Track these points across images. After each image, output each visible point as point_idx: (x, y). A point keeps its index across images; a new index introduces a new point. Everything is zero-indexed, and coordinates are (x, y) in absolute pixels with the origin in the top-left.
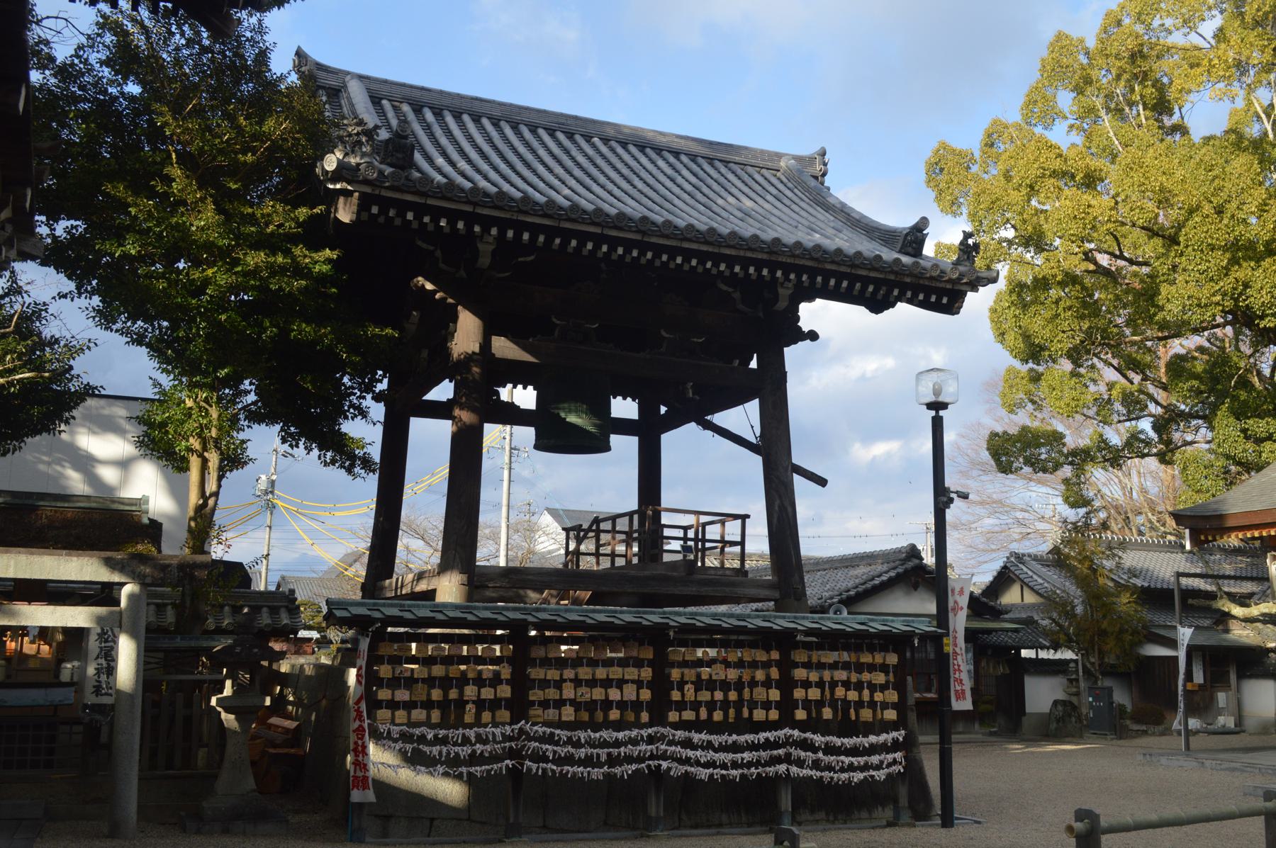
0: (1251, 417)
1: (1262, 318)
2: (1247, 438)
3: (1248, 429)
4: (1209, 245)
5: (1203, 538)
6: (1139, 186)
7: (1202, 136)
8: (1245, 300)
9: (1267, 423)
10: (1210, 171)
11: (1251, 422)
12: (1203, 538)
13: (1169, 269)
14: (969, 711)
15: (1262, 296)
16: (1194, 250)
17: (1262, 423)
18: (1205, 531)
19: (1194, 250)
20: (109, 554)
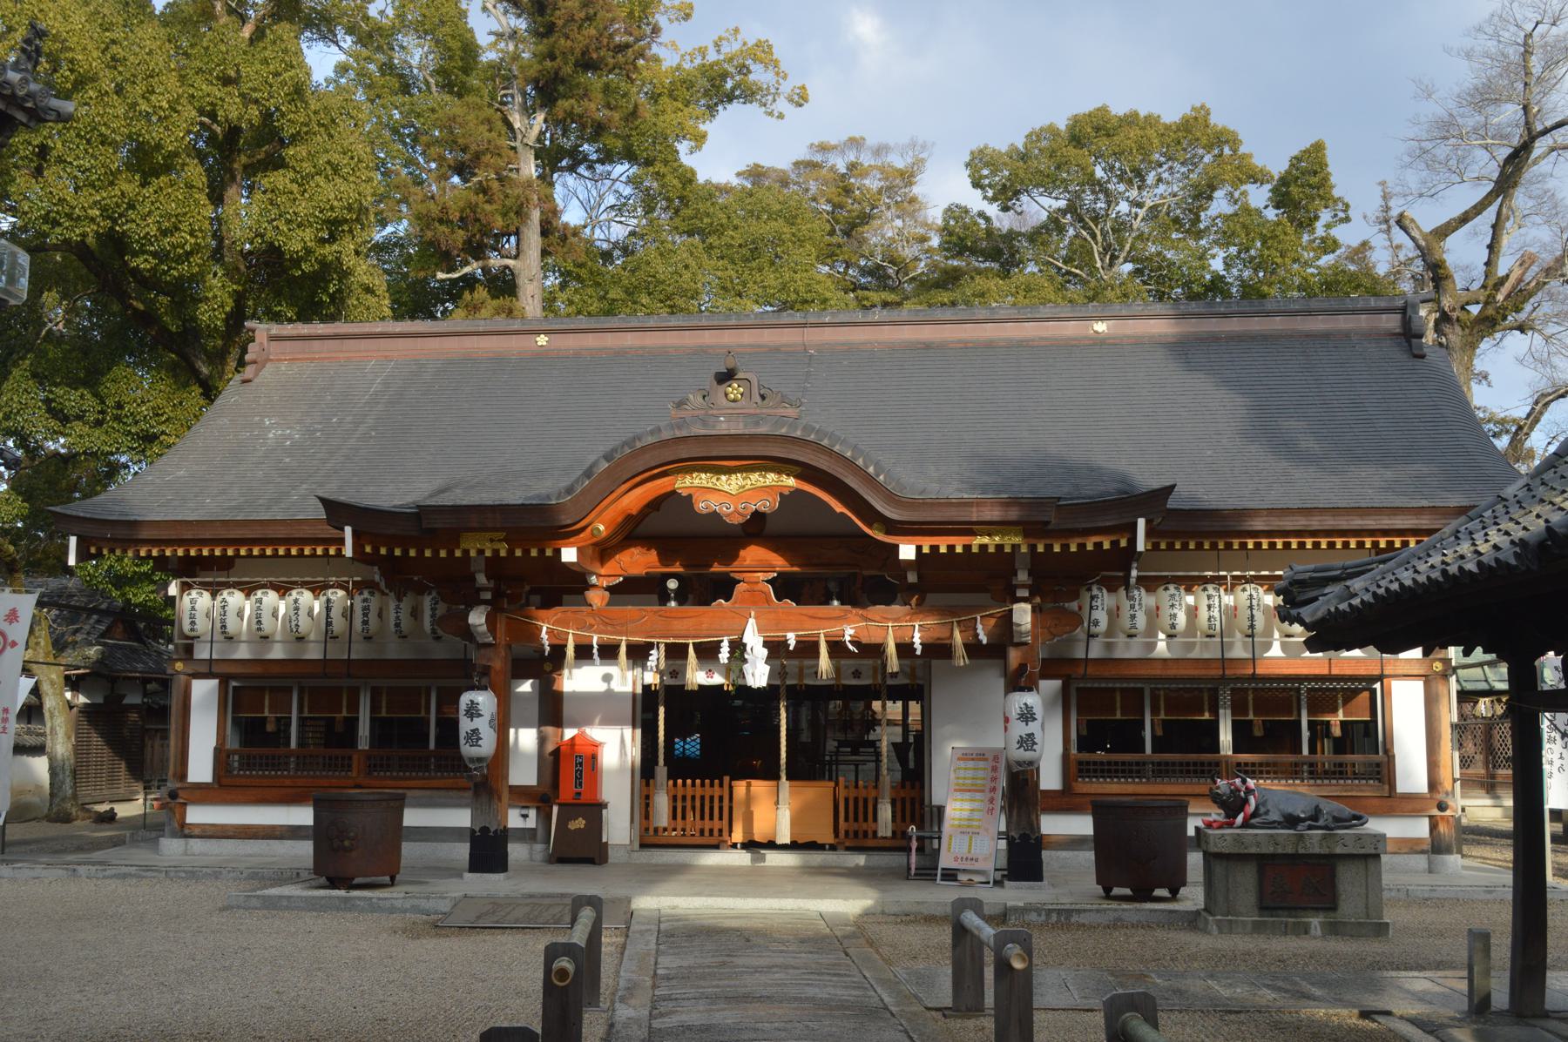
0: (60, 384)
1: (135, 254)
2: (50, 410)
3: (53, 400)
4: (101, 135)
5: (93, 550)
6: (41, 11)
7: (1523, 336)
8: (123, 224)
9: (82, 396)
10: (107, 30)
11: (59, 391)
12: (93, 550)
13: (33, 153)
14: (938, 658)
15: (148, 225)
16: (78, 135)
17: (75, 395)
18: (100, 541)
19: (78, 135)
20: (185, 579)
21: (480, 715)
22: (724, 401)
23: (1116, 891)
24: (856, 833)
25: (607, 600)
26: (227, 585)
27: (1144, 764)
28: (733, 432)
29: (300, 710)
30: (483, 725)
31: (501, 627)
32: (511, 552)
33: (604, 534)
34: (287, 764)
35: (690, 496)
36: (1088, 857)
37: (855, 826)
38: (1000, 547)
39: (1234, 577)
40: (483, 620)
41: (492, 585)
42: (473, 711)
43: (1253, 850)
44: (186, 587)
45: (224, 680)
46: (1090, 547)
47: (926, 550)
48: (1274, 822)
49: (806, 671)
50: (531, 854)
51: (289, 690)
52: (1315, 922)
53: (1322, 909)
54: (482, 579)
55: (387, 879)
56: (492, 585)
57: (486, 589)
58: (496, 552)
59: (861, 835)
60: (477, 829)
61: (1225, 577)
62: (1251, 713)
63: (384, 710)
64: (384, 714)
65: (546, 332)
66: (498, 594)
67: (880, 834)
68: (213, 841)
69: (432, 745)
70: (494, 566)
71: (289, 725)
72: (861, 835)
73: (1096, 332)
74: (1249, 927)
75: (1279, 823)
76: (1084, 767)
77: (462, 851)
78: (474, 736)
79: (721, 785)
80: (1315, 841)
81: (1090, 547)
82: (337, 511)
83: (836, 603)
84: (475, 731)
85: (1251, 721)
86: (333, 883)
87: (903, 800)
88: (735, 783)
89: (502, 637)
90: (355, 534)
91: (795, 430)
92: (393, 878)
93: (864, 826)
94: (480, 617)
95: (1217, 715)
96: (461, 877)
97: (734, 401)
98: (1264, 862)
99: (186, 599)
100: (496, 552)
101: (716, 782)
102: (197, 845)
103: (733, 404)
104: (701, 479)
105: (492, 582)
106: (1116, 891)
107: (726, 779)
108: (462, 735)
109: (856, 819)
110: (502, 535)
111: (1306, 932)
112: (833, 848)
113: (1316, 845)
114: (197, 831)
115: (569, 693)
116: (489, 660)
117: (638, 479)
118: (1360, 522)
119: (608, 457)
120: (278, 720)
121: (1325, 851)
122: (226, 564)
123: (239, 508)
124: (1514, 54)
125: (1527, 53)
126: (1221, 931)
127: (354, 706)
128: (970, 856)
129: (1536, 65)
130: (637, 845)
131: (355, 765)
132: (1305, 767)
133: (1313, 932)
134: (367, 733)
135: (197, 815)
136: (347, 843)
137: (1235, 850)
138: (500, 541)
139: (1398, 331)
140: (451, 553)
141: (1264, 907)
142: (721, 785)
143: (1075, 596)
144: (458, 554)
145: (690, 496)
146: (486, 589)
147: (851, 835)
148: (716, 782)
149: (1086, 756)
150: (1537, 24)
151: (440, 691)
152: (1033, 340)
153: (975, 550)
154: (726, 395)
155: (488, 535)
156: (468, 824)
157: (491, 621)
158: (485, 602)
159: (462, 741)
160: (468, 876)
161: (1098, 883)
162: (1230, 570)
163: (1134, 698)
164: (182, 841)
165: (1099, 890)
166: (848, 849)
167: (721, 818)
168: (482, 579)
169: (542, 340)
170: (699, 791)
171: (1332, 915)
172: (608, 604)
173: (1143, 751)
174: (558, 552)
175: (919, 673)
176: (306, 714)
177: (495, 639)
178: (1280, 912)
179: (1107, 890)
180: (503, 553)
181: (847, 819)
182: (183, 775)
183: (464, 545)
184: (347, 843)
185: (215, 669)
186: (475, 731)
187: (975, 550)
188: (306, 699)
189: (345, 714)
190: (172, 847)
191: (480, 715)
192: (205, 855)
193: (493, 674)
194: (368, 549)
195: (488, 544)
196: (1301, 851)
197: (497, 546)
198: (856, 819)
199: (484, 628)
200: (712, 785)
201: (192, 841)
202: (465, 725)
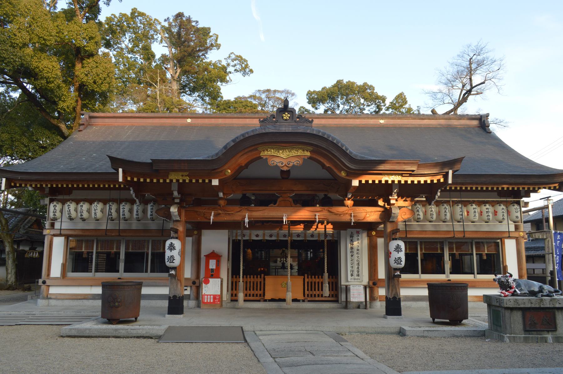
12: (13, 184)
21: (175, 249)
22: (282, 120)
23: (436, 320)
24: (311, 295)
25: (226, 203)
26: (68, 200)
28: (287, 131)
29: (97, 249)
30: (175, 253)
31: (183, 214)
32: (191, 181)
33: (230, 174)
35: (266, 159)
36: (426, 305)
37: (311, 293)
38: (387, 181)
39: (453, 201)
40: (176, 210)
41: (180, 196)
42: (172, 247)
43: (522, 306)
44: (51, 201)
45: (67, 237)
47: (363, 182)
48: (525, 293)
49: (293, 235)
51: (93, 241)
52: (549, 336)
53: (551, 331)
54: (176, 194)
55: (134, 319)
56: (180, 197)
57: (177, 198)
58: (184, 181)
59: (313, 296)
60: (172, 296)
62: (455, 250)
63: (130, 249)
65: (190, 118)
66: (182, 200)
67: (324, 296)
70: (181, 186)
71: (92, 256)
72: (313, 296)
73: (381, 123)
74: (522, 339)
75: (527, 294)
77: (165, 304)
78: (172, 258)
79: (261, 277)
80: (548, 302)
82: (116, 162)
83: (318, 206)
84: (172, 257)
85: (455, 253)
86: (111, 321)
87: (332, 283)
88: (266, 277)
89: (183, 218)
90: (123, 171)
91: (129, 250)
92: (136, 319)
93: (314, 293)
94: (175, 209)
95: (443, 251)
96: (164, 316)
97: (286, 120)
98: (524, 310)
99: (52, 205)
100: (184, 181)
101: (259, 276)
102: (53, 302)
103: (285, 121)
104: (272, 152)
105: (180, 195)
106: (436, 320)
107: (263, 275)
108: (166, 257)
109: (311, 290)
110: (187, 173)
111: (546, 342)
112: (303, 301)
113: (548, 303)
116: (178, 227)
117: (246, 151)
118: (504, 180)
119: (233, 141)
120: (88, 253)
121: (552, 306)
122: (69, 191)
123: (74, 169)
124: (466, 64)
125: (470, 64)
126: (510, 341)
127: (118, 248)
129: (473, 66)
130: (230, 301)
133: (549, 341)
134: (124, 258)
136: (117, 304)
137: (515, 306)
138: (186, 176)
139: (479, 125)
140: (165, 181)
141: (526, 331)
142: (261, 277)
144: (168, 181)
145: (266, 159)
146: (177, 198)
147: (310, 296)
148: (259, 276)
150: (474, 55)
151: (153, 242)
152: (360, 125)
153: (383, 182)
154: (283, 117)
155: (181, 173)
156: (168, 293)
157: (179, 211)
158: (177, 203)
159: (166, 260)
160: (167, 316)
161: (431, 317)
163: (441, 242)
164: (47, 301)
165: (431, 319)
166: (309, 301)
167: (260, 290)
168: (176, 194)
169: (189, 120)
170: (252, 280)
171: (554, 333)
172: (227, 205)
174: (210, 181)
175: (335, 236)
176: (99, 250)
177: (180, 218)
178: (533, 333)
179: (434, 320)
180: (187, 181)
181: (308, 290)
183: (171, 177)
184: (117, 304)
185: (63, 232)
186: (172, 257)
187: (383, 182)
189: (115, 250)
191: (175, 249)
192: (57, 306)
193: (179, 233)
194: (129, 179)
195: (181, 177)
196: (542, 306)
197: (185, 178)
198: (311, 290)
199: (177, 213)
200: (257, 277)
201: (51, 301)
202: (168, 254)
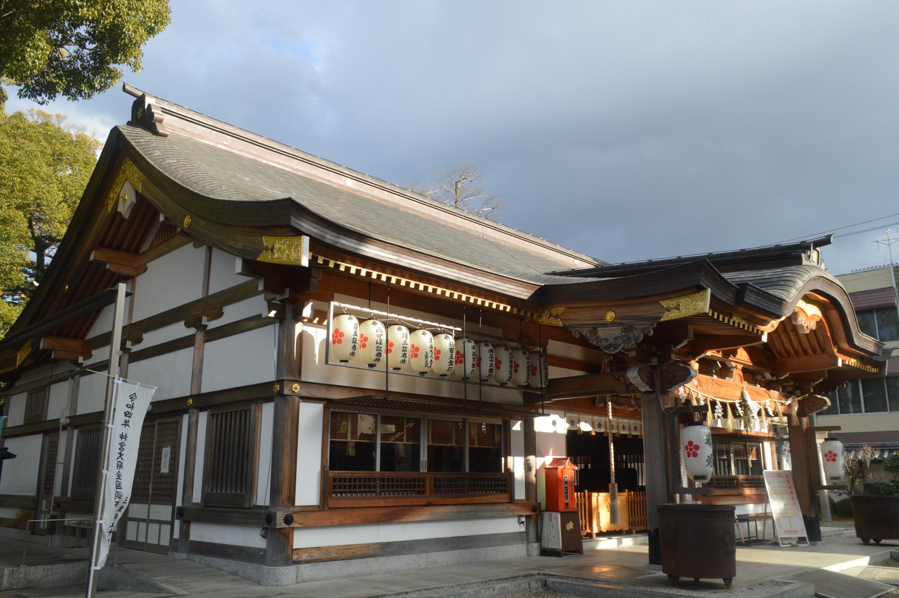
27: (375, 480)
34: (375, 486)
46: (342, 269)
50: (528, 551)
61: (451, 330)
64: (476, 446)
68: (322, 564)
69: (467, 469)
76: (337, 483)
81: (342, 269)
102: (307, 571)
114: (304, 557)
115: (538, 432)
128: (793, 530)
131: (428, 489)
132: (378, 483)
134: (426, 459)
135: (302, 540)
143: (671, 387)
149: (387, 474)
162: (455, 327)
164: (293, 568)
173: (373, 468)
182: (292, 499)
188: (430, 425)
190: (287, 575)
192: (315, 580)
201: (302, 567)
